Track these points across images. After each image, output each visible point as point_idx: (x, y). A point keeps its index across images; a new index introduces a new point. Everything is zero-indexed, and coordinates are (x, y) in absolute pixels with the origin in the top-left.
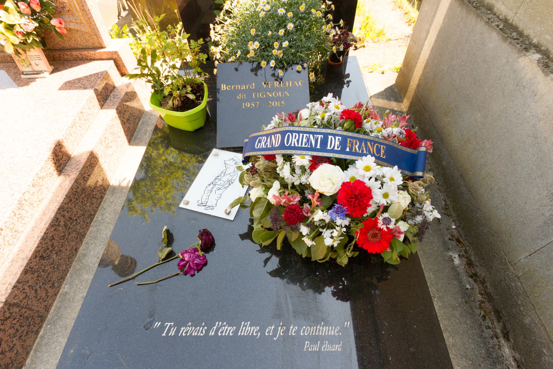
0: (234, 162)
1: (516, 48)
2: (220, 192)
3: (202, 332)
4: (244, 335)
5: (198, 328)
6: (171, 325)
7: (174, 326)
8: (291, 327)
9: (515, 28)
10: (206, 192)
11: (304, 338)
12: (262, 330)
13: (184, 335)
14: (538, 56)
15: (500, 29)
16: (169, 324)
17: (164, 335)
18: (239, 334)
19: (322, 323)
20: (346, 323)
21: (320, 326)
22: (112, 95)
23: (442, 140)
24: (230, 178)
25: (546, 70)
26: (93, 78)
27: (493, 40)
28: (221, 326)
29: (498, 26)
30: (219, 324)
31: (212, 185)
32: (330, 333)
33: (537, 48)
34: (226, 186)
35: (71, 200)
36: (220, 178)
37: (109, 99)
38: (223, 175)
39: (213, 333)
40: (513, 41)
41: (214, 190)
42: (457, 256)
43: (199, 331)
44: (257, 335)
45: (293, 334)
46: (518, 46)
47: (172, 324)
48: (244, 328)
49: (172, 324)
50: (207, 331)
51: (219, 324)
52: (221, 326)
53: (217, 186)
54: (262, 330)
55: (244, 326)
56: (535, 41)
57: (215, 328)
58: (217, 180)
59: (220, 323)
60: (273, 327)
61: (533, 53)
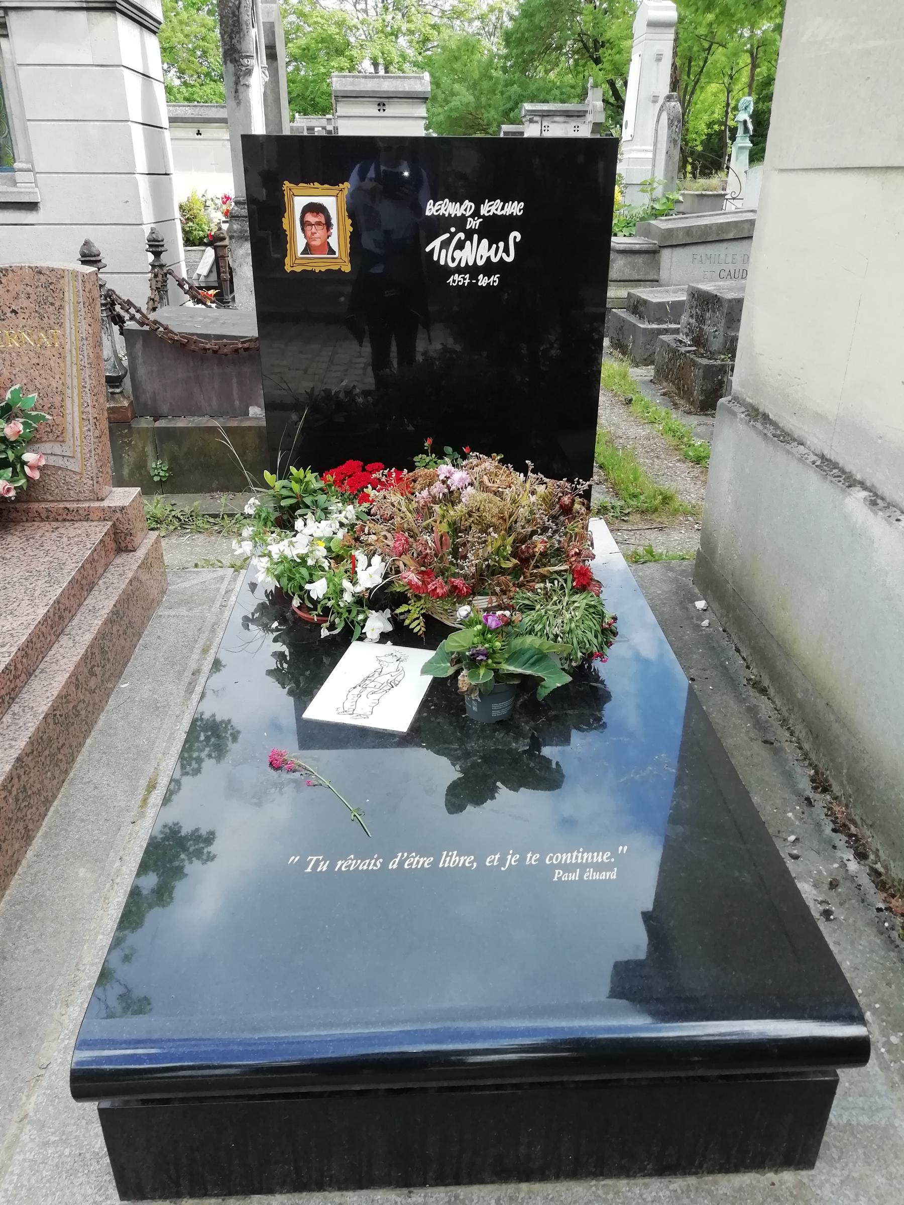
0: (395, 659)
1: (839, 486)
2: (376, 696)
3: (375, 865)
4: (449, 866)
5: (368, 861)
6: (318, 860)
7: (325, 860)
8: (529, 855)
9: (836, 466)
10: (350, 696)
11: (553, 867)
12: (480, 859)
13: (343, 869)
14: (865, 494)
15: (817, 466)
16: (315, 858)
17: (309, 870)
18: (441, 865)
19: (581, 850)
20: (621, 848)
21: (578, 852)
22: (101, 582)
23: (787, 654)
24: (392, 679)
25: (874, 508)
26: (75, 549)
27: (815, 485)
28: (408, 858)
29: (814, 463)
30: (402, 856)
31: (359, 689)
32: (595, 860)
33: (863, 485)
34: (385, 688)
35: (32, 752)
36: (372, 679)
37: (96, 588)
38: (377, 674)
39: (395, 866)
40: (834, 479)
41: (364, 694)
42: (851, 857)
43: (373, 864)
44: (472, 866)
45: (533, 863)
46: (840, 484)
47: (321, 858)
48: (448, 859)
49: (321, 858)
50: (385, 865)
51: (402, 856)
52: (408, 858)
53: (368, 690)
54: (480, 859)
55: (447, 856)
56: (858, 477)
57: (397, 860)
58: (367, 682)
59: (406, 854)
60: (498, 856)
61: (859, 491)
